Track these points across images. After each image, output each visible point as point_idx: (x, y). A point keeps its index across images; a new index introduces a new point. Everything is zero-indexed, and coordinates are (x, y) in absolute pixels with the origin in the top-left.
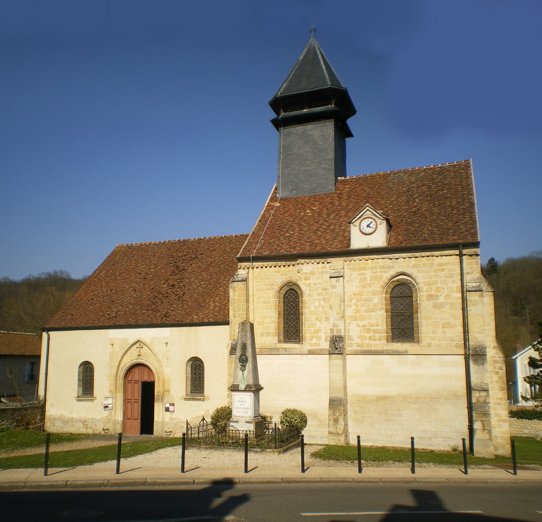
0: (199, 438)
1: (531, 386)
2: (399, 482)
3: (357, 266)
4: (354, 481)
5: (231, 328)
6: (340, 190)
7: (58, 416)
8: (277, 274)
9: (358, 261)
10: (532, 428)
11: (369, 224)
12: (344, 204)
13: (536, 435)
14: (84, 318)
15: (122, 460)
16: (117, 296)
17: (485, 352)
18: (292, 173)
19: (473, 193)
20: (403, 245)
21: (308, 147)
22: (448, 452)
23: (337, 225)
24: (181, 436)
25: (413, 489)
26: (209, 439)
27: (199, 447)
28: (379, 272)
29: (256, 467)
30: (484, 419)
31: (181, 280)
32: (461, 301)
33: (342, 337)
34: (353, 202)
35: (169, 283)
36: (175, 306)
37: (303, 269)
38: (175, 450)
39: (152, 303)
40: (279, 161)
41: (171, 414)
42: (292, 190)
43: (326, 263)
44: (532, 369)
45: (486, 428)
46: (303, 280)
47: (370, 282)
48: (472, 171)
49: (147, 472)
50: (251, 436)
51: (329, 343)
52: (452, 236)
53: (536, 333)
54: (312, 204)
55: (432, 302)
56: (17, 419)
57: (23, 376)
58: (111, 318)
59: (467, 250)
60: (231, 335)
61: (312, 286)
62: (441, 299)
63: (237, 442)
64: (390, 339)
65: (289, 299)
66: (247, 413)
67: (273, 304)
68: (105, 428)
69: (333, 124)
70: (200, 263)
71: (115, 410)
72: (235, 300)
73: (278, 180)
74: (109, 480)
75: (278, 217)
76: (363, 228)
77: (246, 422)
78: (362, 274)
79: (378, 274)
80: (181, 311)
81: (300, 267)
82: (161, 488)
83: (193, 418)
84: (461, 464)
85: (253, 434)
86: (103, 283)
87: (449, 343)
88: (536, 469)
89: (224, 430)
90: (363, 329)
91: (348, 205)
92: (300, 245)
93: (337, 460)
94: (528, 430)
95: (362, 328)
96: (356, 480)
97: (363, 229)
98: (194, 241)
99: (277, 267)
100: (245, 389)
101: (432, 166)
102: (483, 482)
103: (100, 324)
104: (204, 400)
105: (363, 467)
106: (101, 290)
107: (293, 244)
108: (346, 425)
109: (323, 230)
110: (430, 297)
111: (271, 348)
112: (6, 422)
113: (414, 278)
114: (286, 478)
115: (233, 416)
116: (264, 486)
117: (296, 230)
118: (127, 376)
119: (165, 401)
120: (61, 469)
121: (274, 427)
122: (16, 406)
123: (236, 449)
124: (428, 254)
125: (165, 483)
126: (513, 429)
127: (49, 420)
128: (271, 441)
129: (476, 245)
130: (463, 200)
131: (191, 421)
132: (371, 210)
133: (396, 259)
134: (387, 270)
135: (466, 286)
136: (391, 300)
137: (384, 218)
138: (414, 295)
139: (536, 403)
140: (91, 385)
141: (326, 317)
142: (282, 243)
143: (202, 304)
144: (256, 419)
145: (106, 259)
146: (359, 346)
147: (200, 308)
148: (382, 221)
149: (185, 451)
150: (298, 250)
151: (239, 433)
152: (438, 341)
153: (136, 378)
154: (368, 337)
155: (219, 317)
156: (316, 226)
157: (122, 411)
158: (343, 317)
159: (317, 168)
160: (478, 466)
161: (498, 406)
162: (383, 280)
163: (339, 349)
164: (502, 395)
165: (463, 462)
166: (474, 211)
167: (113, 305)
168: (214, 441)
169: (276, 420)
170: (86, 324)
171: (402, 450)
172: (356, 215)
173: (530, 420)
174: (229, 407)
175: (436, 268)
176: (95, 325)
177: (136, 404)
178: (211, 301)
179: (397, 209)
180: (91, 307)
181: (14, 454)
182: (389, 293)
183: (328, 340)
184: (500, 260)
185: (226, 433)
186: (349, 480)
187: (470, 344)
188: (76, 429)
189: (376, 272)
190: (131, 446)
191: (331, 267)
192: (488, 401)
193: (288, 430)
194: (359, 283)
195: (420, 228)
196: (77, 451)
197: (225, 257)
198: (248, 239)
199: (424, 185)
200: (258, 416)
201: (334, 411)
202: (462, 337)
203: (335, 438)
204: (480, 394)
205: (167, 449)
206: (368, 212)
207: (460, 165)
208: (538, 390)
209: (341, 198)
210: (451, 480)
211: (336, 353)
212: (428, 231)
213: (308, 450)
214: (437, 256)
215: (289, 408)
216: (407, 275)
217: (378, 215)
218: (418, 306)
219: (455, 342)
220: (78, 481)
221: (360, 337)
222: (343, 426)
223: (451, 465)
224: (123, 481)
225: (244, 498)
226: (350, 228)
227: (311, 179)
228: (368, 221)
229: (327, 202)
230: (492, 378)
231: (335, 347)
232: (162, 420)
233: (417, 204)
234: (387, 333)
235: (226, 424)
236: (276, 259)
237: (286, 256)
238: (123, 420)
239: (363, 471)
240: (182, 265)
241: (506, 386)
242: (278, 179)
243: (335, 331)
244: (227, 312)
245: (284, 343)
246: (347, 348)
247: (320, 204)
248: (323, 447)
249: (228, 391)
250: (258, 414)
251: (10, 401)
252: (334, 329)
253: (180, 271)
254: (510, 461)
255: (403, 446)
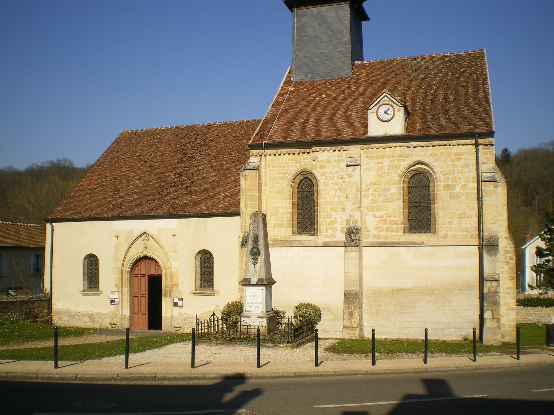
0: (209, 334)
1: (537, 275)
2: (411, 373)
3: (375, 154)
4: (367, 373)
5: (242, 219)
6: (357, 75)
7: (65, 309)
8: (291, 162)
9: (375, 149)
10: (535, 315)
11: (387, 111)
12: (361, 89)
13: (539, 321)
14: (88, 209)
15: (131, 356)
16: (121, 185)
17: (498, 242)
18: (307, 55)
19: (488, 82)
20: (421, 133)
21: (323, 29)
22: (459, 341)
23: (354, 110)
24: (190, 332)
25: (425, 378)
26: (220, 334)
27: (209, 343)
28: (396, 161)
29: (268, 362)
30: (493, 309)
31: (189, 168)
32: (477, 191)
33: (358, 229)
34: (371, 87)
35: (177, 172)
36: (183, 196)
37: (319, 157)
38: (185, 346)
39: (159, 192)
40: (293, 43)
41: (179, 310)
42: (307, 74)
43: (342, 150)
44: (539, 258)
45: (495, 317)
46: (319, 168)
47: (387, 171)
48: (486, 60)
49: (156, 368)
50: (264, 331)
51: (344, 234)
52: (468, 125)
53: (543, 224)
54: (328, 89)
55: (449, 192)
56: (26, 312)
57: (29, 268)
58: (115, 209)
59: (483, 140)
60: (242, 227)
61: (328, 175)
62: (458, 190)
63: (248, 338)
64: (407, 230)
65: (304, 189)
66: (259, 307)
67: (286, 194)
68: (112, 323)
69: (349, 7)
70: (209, 150)
71: (122, 305)
72: (247, 190)
73: (292, 63)
74: (118, 375)
75: (292, 102)
76: (380, 114)
77: (258, 317)
78: (380, 163)
79: (396, 162)
80: (190, 201)
81: (315, 155)
82: (172, 383)
83: (203, 313)
84: (470, 353)
85: (266, 329)
86: (107, 171)
87: (464, 234)
88: (535, 352)
89: (235, 325)
90: (380, 220)
91: (365, 91)
92: (316, 132)
93: (351, 353)
94: (532, 317)
95: (379, 219)
96: (370, 372)
97: (381, 115)
98: (203, 127)
99: (291, 154)
100: (257, 283)
101: (448, 54)
102: (490, 368)
103: (104, 215)
104: (214, 295)
105: (377, 359)
106: (105, 179)
107: (307, 131)
108: (361, 318)
109: (339, 116)
110: (447, 187)
111: (284, 240)
112: (15, 315)
113: (432, 168)
114: (299, 373)
115: (244, 311)
116: (276, 380)
117: (312, 116)
118: (133, 270)
119: (173, 296)
120: (71, 363)
121: (287, 322)
122: (23, 299)
123: (248, 344)
124: (445, 142)
125: (176, 378)
126: (519, 317)
127: (56, 313)
128: (284, 336)
129: (491, 134)
130: (479, 89)
131: (201, 316)
132: (389, 96)
133: (414, 147)
134: (405, 159)
135: (482, 176)
136: (408, 190)
137: (401, 104)
138: (431, 185)
139: (540, 291)
140: (96, 279)
141: (342, 208)
142: (297, 129)
143: (212, 194)
144: (268, 314)
145: (110, 146)
146: (375, 237)
147: (209, 198)
148: (399, 108)
149: (195, 346)
150: (313, 136)
151: (251, 328)
152: (454, 232)
153: (143, 272)
154: (384, 228)
155: (230, 207)
156: (332, 112)
157: (129, 306)
158: (360, 207)
159: (333, 51)
160: (486, 353)
161: (507, 296)
162: (400, 169)
163: (355, 241)
164: (512, 285)
165: (473, 351)
166: (489, 101)
167: (118, 195)
168: (225, 336)
169: (289, 314)
170: (90, 215)
171: (416, 342)
172: (374, 100)
173: (534, 307)
174: (240, 302)
175: (453, 157)
176: (100, 216)
177: (143, 299)
178: (221, 190)
179: (415, 96)
180: (95, 197)
181: (24, 346)
182: (407, 183)
183: (344, 232)
184: (513, 151)
185: (237, 329)
186: (362, 372)
187: (484, 234)
188: (83, 323)
189: (394, 161)
190: (139, 341)
191: (347, 155)
192: (498, 291)
193: (301, 325)
194: (377, 172)
195: (437, 116)
196: (85, 345)
197: (236, 143)
198: (260, 125)
199: (441, 72)
200: (271, 311)
201: (349, 304)
202: (477, 227)
203: (349, 331)
204: (491, 284)
205: (176, 345)
206: (385, 98)
207: (475, 54)
208: (542, 278)
209: (358, 83)
210: (460, 368)
211: (352, 245)
212: (446, 119)
213: (322, 345)
214: (454, 145)
215: (303, 302)
216: (425, 164)
217: (396, 102)
218: (436, 197)
219: (471, 232)
220: (87, 374)
221: (377, 228)
222: (357, 319)
223: (462, 354)
224: (132, 376)
225: (256, 393)
226: (367, 115)
227: (327, 62)
228: (386, 107)
229: (343, 87)
230: (503, 268)
231: (351, 238)
232: (170, 315)
233: (434, 91)
234: (404, 224)
235: (237, 319)
236: (291, 146)
237: (301, 143)
238: (130, 315)
239: (376, 364)
240: (190, 152)
241: (515, 275)
242: (293, 62)
243: (351, 222)
244: (238, 202)
245: (298, 235)
246: (364, 240)
247: (337, 89)
248: (337, 341)
249: (239, 286)
250: (271, 309)
251: (17, 293)
252: (350, 220)
253: (188, 158)
254: (515, 347)
255: (417, 338)
